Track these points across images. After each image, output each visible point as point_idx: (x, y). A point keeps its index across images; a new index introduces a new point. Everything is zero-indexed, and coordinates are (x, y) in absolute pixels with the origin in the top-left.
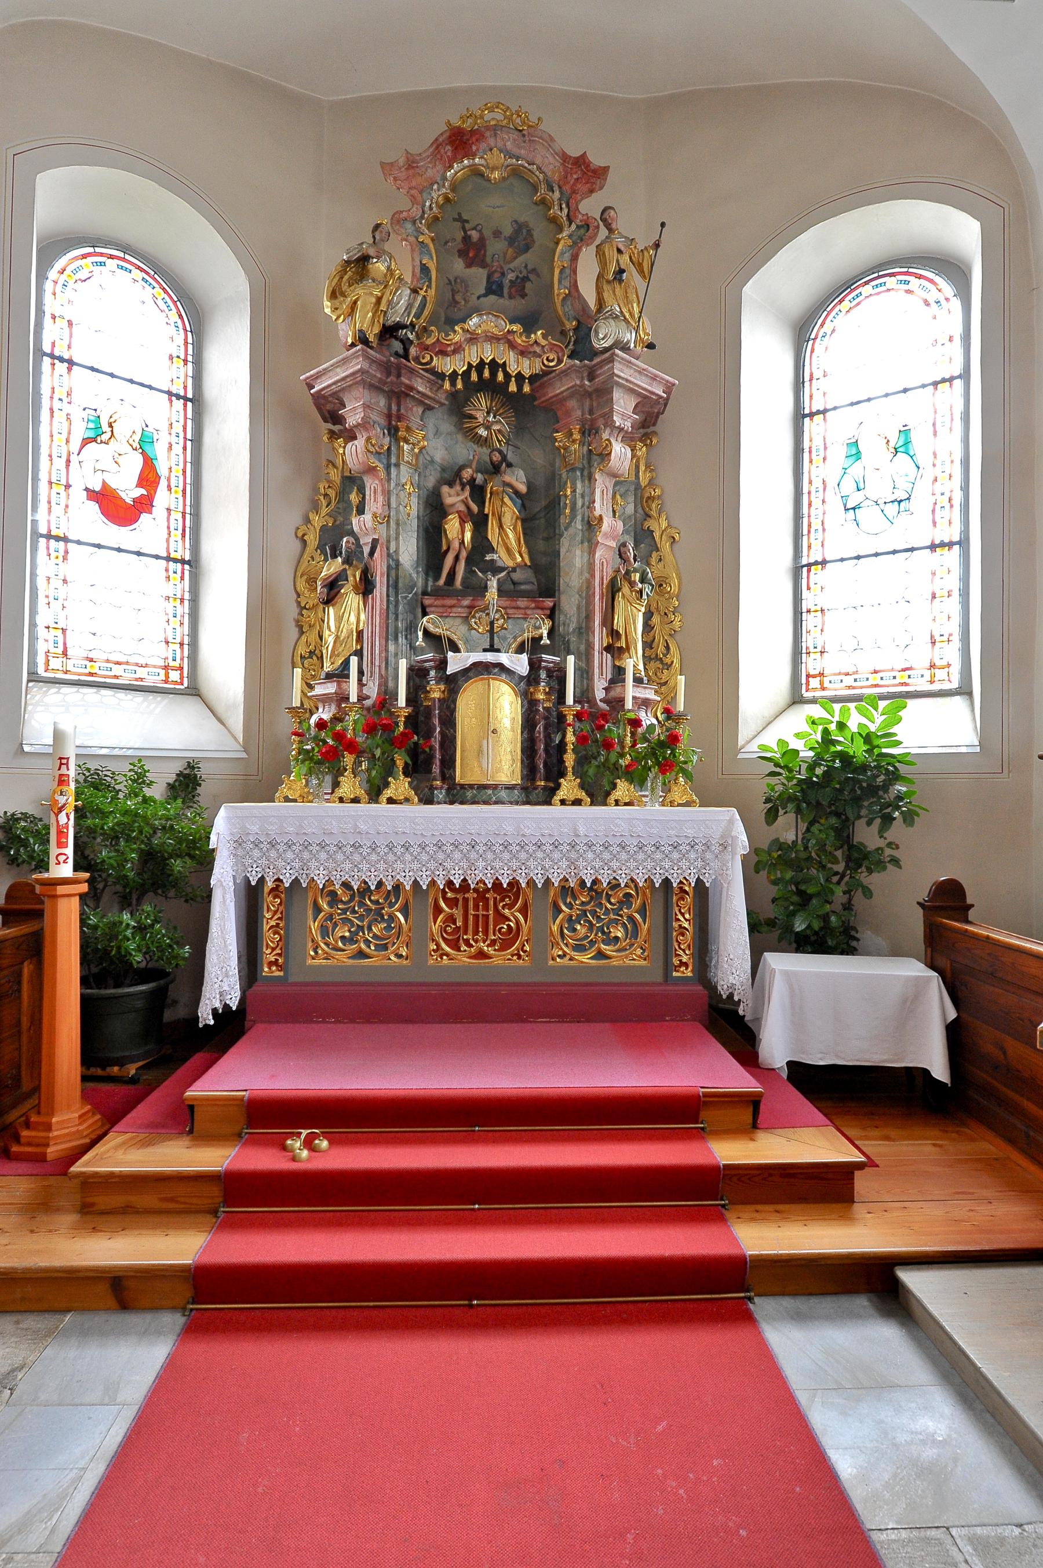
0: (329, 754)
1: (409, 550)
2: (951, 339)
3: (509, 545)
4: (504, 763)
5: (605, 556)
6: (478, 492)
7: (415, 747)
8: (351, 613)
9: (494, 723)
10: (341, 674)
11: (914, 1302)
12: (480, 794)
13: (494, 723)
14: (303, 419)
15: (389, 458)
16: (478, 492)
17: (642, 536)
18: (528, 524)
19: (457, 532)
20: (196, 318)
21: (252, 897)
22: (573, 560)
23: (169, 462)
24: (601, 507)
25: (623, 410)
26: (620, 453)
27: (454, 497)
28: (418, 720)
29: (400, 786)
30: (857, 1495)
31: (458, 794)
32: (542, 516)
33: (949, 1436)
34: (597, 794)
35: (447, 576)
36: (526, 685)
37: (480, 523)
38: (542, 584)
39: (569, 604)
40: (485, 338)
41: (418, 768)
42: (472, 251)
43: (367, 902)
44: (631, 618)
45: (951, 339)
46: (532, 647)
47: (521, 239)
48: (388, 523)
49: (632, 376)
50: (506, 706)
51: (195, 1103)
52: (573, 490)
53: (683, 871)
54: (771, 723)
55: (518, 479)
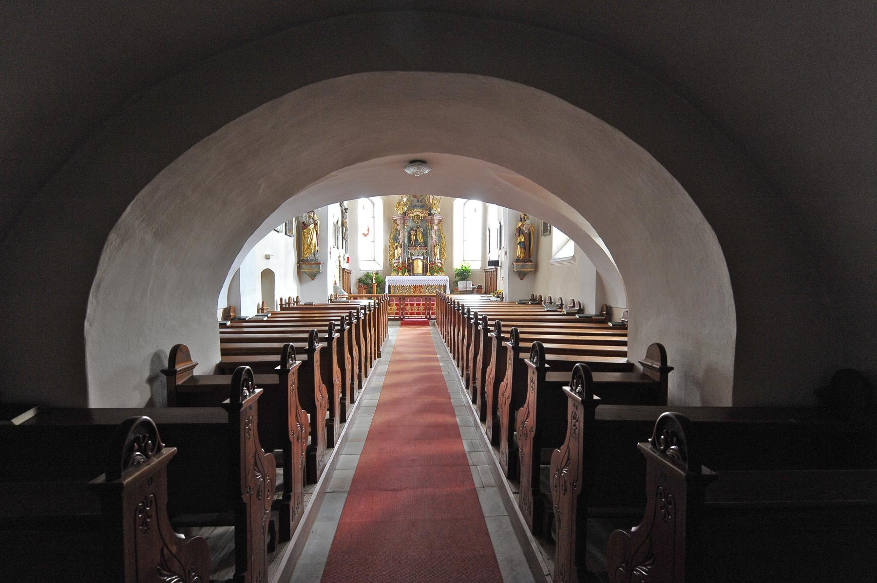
1: (406, 241)
4: (420, 271)
5: (434, 243)
6: (416, 231)
7: (408, 268)
8: (398, 251)
9: (419, 265)
10: (398, 259)
11: (531, 524)
12: (417, 274)
13: (419, 265)
14: (391, 224)
16: (416, 231)
17: (440, 236)
19: (413, 237)
21: (389, 287)
22: (429, 242)
24: (433, 235)
25: (436, 222)
26: (436, 227)
27: (412, 233)
28: (409, 264)
29: (407, 274)
30: (603, 373)
31: (414, 275)
32: (425, 235)
33: (412, 201)
34: (432, 274)
35: (412, 244)
37: (416, 235)
39: (429, 248)
40: (416, 212)
41: (409, 271)
42: (415, 196)
43: (403, 287)
44: (437, 251)
48: (403, 237)
49: (437, 218)
50: (420, 263)
53: (442, 284)
54: (457, 265)
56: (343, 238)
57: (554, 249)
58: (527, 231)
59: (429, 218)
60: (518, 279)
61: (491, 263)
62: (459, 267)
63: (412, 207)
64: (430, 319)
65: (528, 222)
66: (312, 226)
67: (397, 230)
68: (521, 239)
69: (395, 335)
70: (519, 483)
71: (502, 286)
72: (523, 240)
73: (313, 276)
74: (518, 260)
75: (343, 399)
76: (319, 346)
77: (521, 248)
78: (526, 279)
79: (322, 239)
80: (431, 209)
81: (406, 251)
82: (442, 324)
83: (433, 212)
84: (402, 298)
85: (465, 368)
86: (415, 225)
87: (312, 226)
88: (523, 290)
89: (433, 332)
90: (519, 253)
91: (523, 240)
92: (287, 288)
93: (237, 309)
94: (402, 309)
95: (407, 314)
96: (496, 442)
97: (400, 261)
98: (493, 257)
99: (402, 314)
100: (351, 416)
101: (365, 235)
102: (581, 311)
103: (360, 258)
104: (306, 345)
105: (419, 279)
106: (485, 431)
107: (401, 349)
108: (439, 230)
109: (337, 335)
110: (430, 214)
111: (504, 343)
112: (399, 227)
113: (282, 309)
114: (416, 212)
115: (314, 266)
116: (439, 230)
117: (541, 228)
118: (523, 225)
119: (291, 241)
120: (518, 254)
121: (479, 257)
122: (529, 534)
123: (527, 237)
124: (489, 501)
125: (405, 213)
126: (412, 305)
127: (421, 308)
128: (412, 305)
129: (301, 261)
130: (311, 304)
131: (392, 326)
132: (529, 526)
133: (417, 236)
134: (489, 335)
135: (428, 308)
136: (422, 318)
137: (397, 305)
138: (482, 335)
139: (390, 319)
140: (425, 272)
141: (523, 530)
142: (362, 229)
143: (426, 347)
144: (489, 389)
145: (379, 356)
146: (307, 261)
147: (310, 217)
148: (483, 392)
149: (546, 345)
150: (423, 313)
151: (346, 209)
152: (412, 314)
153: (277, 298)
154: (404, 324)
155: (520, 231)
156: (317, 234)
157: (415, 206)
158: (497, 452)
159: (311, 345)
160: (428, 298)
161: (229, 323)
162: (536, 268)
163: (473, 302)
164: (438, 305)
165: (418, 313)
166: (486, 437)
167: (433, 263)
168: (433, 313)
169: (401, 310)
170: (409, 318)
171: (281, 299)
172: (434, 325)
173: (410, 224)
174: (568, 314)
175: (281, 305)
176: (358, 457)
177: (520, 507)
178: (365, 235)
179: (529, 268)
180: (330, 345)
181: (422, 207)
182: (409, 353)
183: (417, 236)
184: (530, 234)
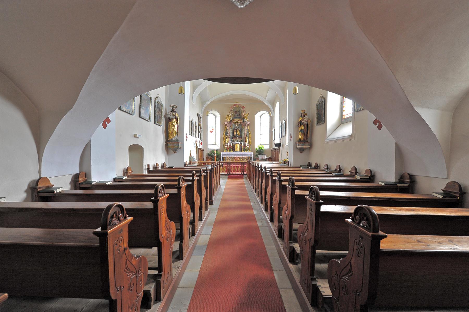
0: (227, 150)
1: (231, 135)
2: (136, 136)
3: (238, 133)
4: (238, 149)
7: (232, 148)
8: (228, 140)
11: (310, 299)
12: (237, 151)
14: (223, 125)
15: (230, 128)
17: (248, 133)
18: (240, 132)
19: (235, 133)
20: (216, 117)
21: (223, 157)
22: (243, 135)
23: (214, 129)
24: (245, 131)
25: (246, 125)
26: (246, 128)
27: (235, 130)
28: (233, 146)
32: (241, 132)
33: (235, 115)
36: (240, 144)
38: (241, 137)
39: (243, 138)
41: (233, 150)
42: (236, 112)
43: (230, 158)
44: (247, 140)
45: (136, 136)
46: (240, 141)
47: (239, 112)
48: (230, 133)
49: (247, 123)
50: (238, 146)
51: (243, 104)
52: (243, 130)
54: (257, 146)
55: (239, 129)
56: (199, 132)
57: (328, 132)
58: (306, 123)
59: (243, 123)
60: (299, 153)
61: (277, 145)
62: (258, 148)
63: (234, 118)
64: (244, 175)
65: (306, 117)
66: (174, 120)
67: (227, 129)
68: (302, 128)
69: (224, 184)
70: (283, 239)
71: (283, 156)
72: (303, 128)
73: (175, 150)
74: (300, 141)
75: (201, 208)
76: (196, 178)
77: (302, 133)
78: (304, 153)
79: (181, 127)
80: (244, 119)
81: (231, 140)
82: (251, 178)
83: (245, 120)
84: (229, 163)
85: (260, 194)
86: (236, 127)
87: (174, 120)
88: (303, 159)
89: (245, 182)
90: (300, 136)
91: (303, 128)
92: (155, 158)
93: (87, 175)
94: (229, 169)
95: (231, 171)
96: (272, 220)
97: (229, 145)
98: (277, 141)
99: (229, 171)
100: (198, 231)
101: (211, 132)
102: (371, 177)
103: (209, 143)
104: (191, 178)
105: (238, 154)
106: (267, 216)
107: (227, 197)
108: (248, 129)
109: (203, 174)
110: (243, 121)
111: (283, 183)
112: (228, 128)
113: (149, 171)
114: (237, 120)
115: (175, 144)
116: (248, 130)
117: (315, 121)
118: (303, 119)
119: (160, 129)
120: (300, 137)
121: (268, 142)
122: (269, 221)
123: (306, 127)
124: (279, 276)
125: (231, 121)
126: (234, 167)
127: (239, 169)
128: (234, 167)
129: (167, 141)
130: (172, 168)
131: (223, 178)
132: (287, 256)
133: (238, 124)
134: (267, 174)
135: (243, 169)
136: (239, 174)
137: (226, 167)
138: (264, 174)
139: (221, 175)
140: (241, 150)
141: (274, 235)
142: (210, 129)
143: (243, 195)
144: (268, 198)
145: (211, 203)
146: (171, 141)
147: (173, 115)
148: (261, 193)
149: (323, 193)
150: (240, 171)
151: (201, 117)
152: (234, 171)
153: (145, 164)
154: (230, 177)
155: (301, 123)
156: (178, 126)
157: (236, 118)
158: (282, 243)
159: (193, 178)
160: (243, 163)
161: (125, 178)
162: (311, 146)
163: (266, 164)
164: (249, 168)
165: (237, 171)
166: (274, 232)
167: (245, 146)
168: (245, 171)
169: (228, 170)
170: (232, 174)
171: (148, 165)
172: (246, 178)
173: (233, 126)
174: (361, 181)
175: (148, 168)
176: (197, 273)
177: (284, 249)
178: (211, 132)
179: (306, 145)
180: (193, 183)
181: (239, 118)
182: (233, 200)
183: (238, 124)
184: (307, 125)
